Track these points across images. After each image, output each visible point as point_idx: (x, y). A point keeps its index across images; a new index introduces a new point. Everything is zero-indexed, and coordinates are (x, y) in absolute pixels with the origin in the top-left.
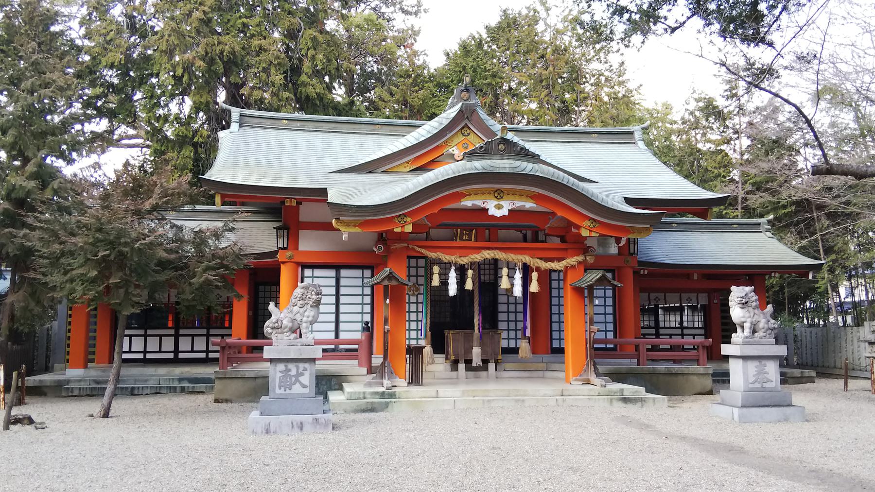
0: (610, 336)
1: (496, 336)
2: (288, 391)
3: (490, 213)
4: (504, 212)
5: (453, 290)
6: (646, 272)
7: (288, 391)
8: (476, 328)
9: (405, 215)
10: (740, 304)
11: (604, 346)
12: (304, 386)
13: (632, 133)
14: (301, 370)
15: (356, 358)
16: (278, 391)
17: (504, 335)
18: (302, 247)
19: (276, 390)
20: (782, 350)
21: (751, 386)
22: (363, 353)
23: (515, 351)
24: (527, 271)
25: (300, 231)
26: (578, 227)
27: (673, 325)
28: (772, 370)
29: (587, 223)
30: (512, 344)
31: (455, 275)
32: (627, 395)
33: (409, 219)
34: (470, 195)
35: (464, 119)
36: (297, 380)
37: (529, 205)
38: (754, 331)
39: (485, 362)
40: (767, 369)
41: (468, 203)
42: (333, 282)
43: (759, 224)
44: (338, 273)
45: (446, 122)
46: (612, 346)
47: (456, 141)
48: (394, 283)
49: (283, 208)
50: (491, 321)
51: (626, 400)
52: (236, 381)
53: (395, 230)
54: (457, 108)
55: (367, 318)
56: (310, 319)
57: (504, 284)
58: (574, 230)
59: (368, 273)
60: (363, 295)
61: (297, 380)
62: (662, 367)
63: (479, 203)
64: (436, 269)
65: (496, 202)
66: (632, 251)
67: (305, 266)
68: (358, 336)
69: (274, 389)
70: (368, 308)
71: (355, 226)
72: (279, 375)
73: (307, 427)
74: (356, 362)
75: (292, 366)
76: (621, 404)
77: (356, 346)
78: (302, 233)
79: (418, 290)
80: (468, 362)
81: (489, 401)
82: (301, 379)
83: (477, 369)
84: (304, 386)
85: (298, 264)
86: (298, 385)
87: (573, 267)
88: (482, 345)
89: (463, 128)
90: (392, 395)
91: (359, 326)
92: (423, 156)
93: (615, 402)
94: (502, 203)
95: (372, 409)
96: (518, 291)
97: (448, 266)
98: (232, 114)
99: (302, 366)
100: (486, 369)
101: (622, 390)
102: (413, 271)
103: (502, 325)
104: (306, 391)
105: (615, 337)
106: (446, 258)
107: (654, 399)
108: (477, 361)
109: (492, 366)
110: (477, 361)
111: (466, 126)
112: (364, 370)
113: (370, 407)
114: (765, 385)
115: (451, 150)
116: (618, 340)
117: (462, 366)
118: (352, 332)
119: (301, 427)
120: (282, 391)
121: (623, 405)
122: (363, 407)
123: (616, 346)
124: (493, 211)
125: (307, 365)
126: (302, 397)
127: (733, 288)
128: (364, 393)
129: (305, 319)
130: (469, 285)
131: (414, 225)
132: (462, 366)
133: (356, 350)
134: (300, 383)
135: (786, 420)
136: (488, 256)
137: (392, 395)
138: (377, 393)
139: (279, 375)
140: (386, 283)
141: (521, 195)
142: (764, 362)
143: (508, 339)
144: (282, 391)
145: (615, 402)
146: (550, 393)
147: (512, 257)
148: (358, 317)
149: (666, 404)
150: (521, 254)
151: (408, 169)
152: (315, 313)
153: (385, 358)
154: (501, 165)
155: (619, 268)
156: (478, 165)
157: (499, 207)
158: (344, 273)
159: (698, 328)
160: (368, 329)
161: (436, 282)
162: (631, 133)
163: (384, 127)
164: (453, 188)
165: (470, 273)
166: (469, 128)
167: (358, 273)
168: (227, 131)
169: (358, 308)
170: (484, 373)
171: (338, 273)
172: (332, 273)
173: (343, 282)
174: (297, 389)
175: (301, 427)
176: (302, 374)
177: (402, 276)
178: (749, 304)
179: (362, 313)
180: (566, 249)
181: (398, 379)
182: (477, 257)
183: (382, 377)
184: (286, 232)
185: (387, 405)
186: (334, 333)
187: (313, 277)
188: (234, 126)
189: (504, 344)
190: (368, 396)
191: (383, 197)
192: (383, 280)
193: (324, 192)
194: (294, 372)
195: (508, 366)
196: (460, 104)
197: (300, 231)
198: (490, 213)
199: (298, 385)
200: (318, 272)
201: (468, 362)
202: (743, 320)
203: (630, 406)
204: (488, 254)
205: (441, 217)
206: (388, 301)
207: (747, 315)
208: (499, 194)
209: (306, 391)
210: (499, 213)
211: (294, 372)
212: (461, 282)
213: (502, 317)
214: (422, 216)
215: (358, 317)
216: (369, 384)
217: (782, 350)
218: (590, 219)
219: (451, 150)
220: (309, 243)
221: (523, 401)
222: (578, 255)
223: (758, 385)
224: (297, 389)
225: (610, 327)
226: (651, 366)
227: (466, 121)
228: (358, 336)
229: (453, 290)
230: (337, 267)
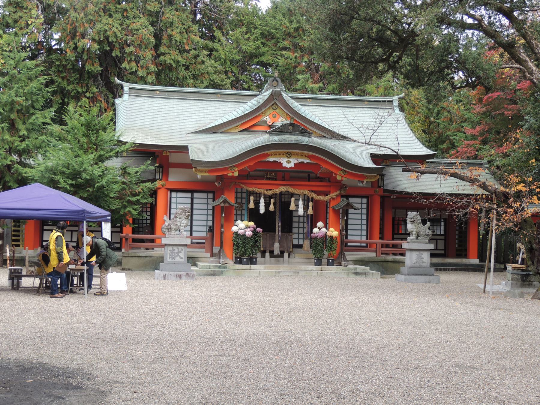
0: (364, 238)
1: (289, 237)
2: (173, 260)
3: (283, 166)
4: (292, 165)
5: (262, 210)
6: (395, 197)
7: (173, 260)
8: (277, 231)
9: (234, 166)
10: (413, 223)
11: (359, 244)
12: (181, 258)
13: (391, 101)
14: (180, 250)
15: (204, 247)
16: (168, 260)
17: (295, 236)
18: (170, 179)
19: (168, 259)
20: (432, 246)
21: (414, 265)
22: (207, 245)
23: (300, 246)
24: (307, 200)
25: (170, 169)
26: (336, 174)
27: (439, 233)
28: (426, 256)
29: (340, 172)
30: (301, 242)
31: (263, 201)
32: (358, 271)
33: (236, 169)
34: (272, 155)
35: (274, 100)
36: (178, 255)
37: (306, 161)
38: (418, 236)
39: (282, 252)
40: (423, 256)
41: (271, 160)
42: (189, 201)
43: (482, 164)
44: (192, 196)
45: (262, 102)
46: (364, 245)
47: (269, 112)
48: (227, 205)
49: (160, 158)
50: (287, 228)
51: (357, 274)
52: (134, 258)
53: (229, 175)
54: (269, 92)
55: (210, 223)
56: (185, 224)
57: (292, 207)
58: (334, 175)
59: (211, 196)
60: (207, 209)
61: (178, 255)
62: (390, 258)
63: (278, 160)
64: (252, 198)
65: (287, 159)
66: (380, 185)
67: (172, 190)
68: (204, 234)
69: (167, 259)
70: (210, 218)
71: (205, 172)
72: (169, 252)
73: (183, 277)
74: (203, 250)
75: (175, 248)
76: (353, 276)
77: (204, 241)
78: (171, 170)
79: (242, 207)
80: (272, 252)
81: (279, 272)
82: (179, 254)
83: (277, 256)
84: (181, 258)
85: (168, 189)
86: (178, 257)
87: (333, 199)
88: (280, 242)
89: (273, 105)
90: (225, 268)
91: (205, 229)
92: (246, 124)
93: (350, 274)
94: (290, 160)
95: (214, 274)
96: (301, 212)
97: (258, 195)
98: (124, 88)
99: (180, 248)
100: (283, 257)
101: (356, 268)
102: (239, 195)
103: (295, 230)
104: (183, 260)
105: (367, 239)
106: (257, 190)
107: (373, 273)
108: (277, 251)
109: (286, 255)
110: (277, 251)
111: (275, 103)
112: (208, 255)
113: (213, 273)
114: (421, 264)
115: (265, 119)
116: (368, 241)
117: (268, 254)
118: (201, 232)
119: (180, 276)
120: (170, 260)
121: (355, 276)
122: (209, 273)
123: (367, 244)
124: (285, 164)
125: (183, 248)
126: (180, 263)
127: (409, 213)
128: (209, 266)
129: (182, 225)
130: (272, 208)
131: (239, 171)
132: (268, 254)
133: (204, 243)
134: (180, 256)
135: (429, 282)
136: (283, 190)
137: (225, 268)
138: (217, 266)
139: (169, 252)
140: (222, 205)
141: (302, 155)
142: (421, 252)
143: (298, 239)
144: (170, 260)
145: (350, 274)
146: (314, 269)
147: (297, 191)
148: (205, 223)
149: (380, 276)
150: (304, 189)
151: (238, 130)
152: (180, 220)
153: (221, 247)
154: (290, 139)
155: (371, 196)
156: (276, 139)
157: (289, 162)
158: (196, 195)
159: (441, 235)
160: (211, 230)
161: (252, 205)
162: (391, 101)
163: (223, 96)
164: (262, 152)
165: (272, 201)
166: (277, 105)
167: (204, 195)
168: (120, 99)
169: (205, 218)
170: (282, 259)
171: (192, 196)
172: (189, 195)
173: (195, 201)
174: (178, 259)
175: (180, 276)
176: (180, 252)
177: (232, 201)
178: (415, 222)
179: (207, 220)
180: (330, 186)
181: (228, 260)
182: (277, 191)
183: (220, 258)
184: (161, 169)
185: (222, 272)
186: (189, 232)
187: (177, 197)
188: (126, 97)
189: (295, 242)
190: (211, 268)
191: (222, 156)
192: (221, 203)
193: (184, 149)
194: (176, 251)
195: (296, 255)
196: (271, 90)
197: (170, 169)
198: (283, 166)
199: (178, 257)
200: (180, 195)
201: (272, 252)
202: (412, 230)
203: (358, 277)
204: (283, 189)
205: (255, 168)
206: (223, 215)
207: (414, 227)
208: (289, 155)
209: (183, 260)
210: (288, 166)
211: (176, 251)
212: (267, 205)
213: (295, 225)
214: (245, 167)
215: (205, 223)
216: (212, 262)
217: (432, 246)
218: (342, 170)
219: (265, 119)
220: (175, 177)
221: (298, 272)
222: (336, 191)
223: (417, 265)
224: (178, 259)
225: (364, 233)
226: (384, 257)
227: (275, 100)
228: (204, 234)
229: (262, 210)
230: (192, 192)
